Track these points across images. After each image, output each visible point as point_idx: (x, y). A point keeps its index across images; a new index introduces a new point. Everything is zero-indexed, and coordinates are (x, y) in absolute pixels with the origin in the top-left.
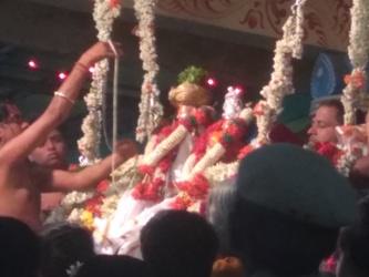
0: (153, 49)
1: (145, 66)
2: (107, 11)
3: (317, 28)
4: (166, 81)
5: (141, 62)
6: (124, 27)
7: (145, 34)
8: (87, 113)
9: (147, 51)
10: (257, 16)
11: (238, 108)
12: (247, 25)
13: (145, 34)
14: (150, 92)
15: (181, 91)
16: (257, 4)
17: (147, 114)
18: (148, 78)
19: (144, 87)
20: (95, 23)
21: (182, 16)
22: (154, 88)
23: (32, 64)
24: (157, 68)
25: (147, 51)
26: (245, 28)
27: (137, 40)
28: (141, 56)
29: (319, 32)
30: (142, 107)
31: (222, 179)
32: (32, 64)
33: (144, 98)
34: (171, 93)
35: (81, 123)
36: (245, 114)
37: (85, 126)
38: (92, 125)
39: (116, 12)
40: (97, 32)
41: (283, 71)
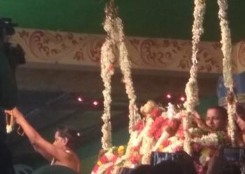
0: (132, 88)
1: (129, 97)
2: (107, 73)
3: (216, 64)
4: (140, 103)
5: (127, 95)
6: (117, 78)
7: (127, 81)
8: (103, 123)
9: (129, 89)
10: (185, 62)
11: (175, 113)
12: (76, 59)
13: (127, 81)
14: (133, 109)
15: (147, 107)
16: (184, 57)
17: (133, 120)
18: (132, 102)
19: (130, 107)
20: (102, 79)
21: (149, 67)
22: (135, 107)
23: (80, 99)
24: (135, 97)
25: (129, 89)
26: (75, 62)
27: (124, 85)
28: (127, 92)
29: (217, 66)
30: (131, 117)
31: (221, 105)
32: (80, 99)
33: (131, 112)
34: (142, 109)
35: (101, 128)
36: (177, 116)
37: (103, 130)
38: (107, 129)
39: (112, 72)
40: (103, 83)
41: (193, 95)
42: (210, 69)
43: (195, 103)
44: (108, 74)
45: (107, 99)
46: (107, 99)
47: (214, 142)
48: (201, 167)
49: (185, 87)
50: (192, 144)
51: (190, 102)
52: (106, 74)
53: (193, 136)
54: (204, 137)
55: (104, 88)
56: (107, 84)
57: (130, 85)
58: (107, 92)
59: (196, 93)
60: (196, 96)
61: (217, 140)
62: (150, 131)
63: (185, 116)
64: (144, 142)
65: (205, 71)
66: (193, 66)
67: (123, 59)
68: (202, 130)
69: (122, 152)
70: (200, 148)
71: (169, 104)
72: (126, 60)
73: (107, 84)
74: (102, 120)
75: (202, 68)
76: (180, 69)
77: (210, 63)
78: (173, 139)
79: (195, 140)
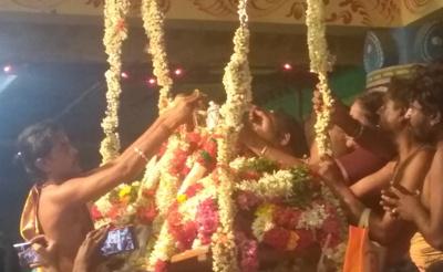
7: (156, 50)
13: (156, 50)
29: (362, 13)
39: (124, 35)
41: (238, 92)
42: (348, 19)
43: (242, 107)
44: (116, 38)
45: (113, 89)
46: (113, 89)
47: (285, 189)
48: (253, 243)
49: (222, 74)
50: (236, 195)
51: (232, 106)
52: (112, 40)
53: (241, 176)
54: (266, 179)
55: (108, 66)
56: (114, 59)
57: (161, 57)
58: (113, 74)
59: (247, 85)
60: (245, 92)
61: (289, 185)
62: (172, 162)
63: (221, 136)
64: (162, 183)
65: (340, 22)
66: (240, 29)
67: (148, 7)
68: (263, 163)
69: (128, 198)
70: (252, 203)
71: (211, 103)
72: (154, 9)
73: (114, 59)
74: (102, 129)
75: (334, 16)
76: (292, 20)
77: (348, 8)
78: (207, 181)
79: (243, 186)
